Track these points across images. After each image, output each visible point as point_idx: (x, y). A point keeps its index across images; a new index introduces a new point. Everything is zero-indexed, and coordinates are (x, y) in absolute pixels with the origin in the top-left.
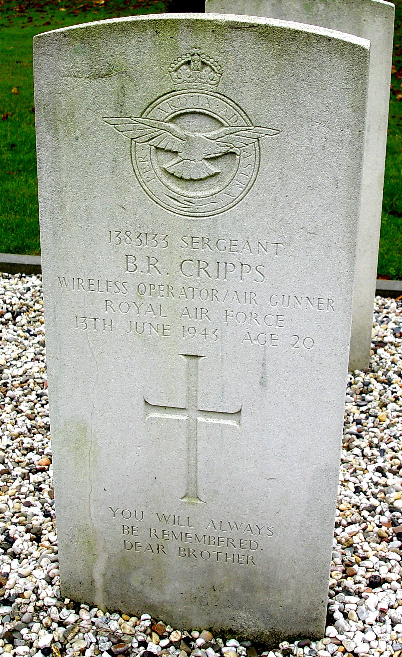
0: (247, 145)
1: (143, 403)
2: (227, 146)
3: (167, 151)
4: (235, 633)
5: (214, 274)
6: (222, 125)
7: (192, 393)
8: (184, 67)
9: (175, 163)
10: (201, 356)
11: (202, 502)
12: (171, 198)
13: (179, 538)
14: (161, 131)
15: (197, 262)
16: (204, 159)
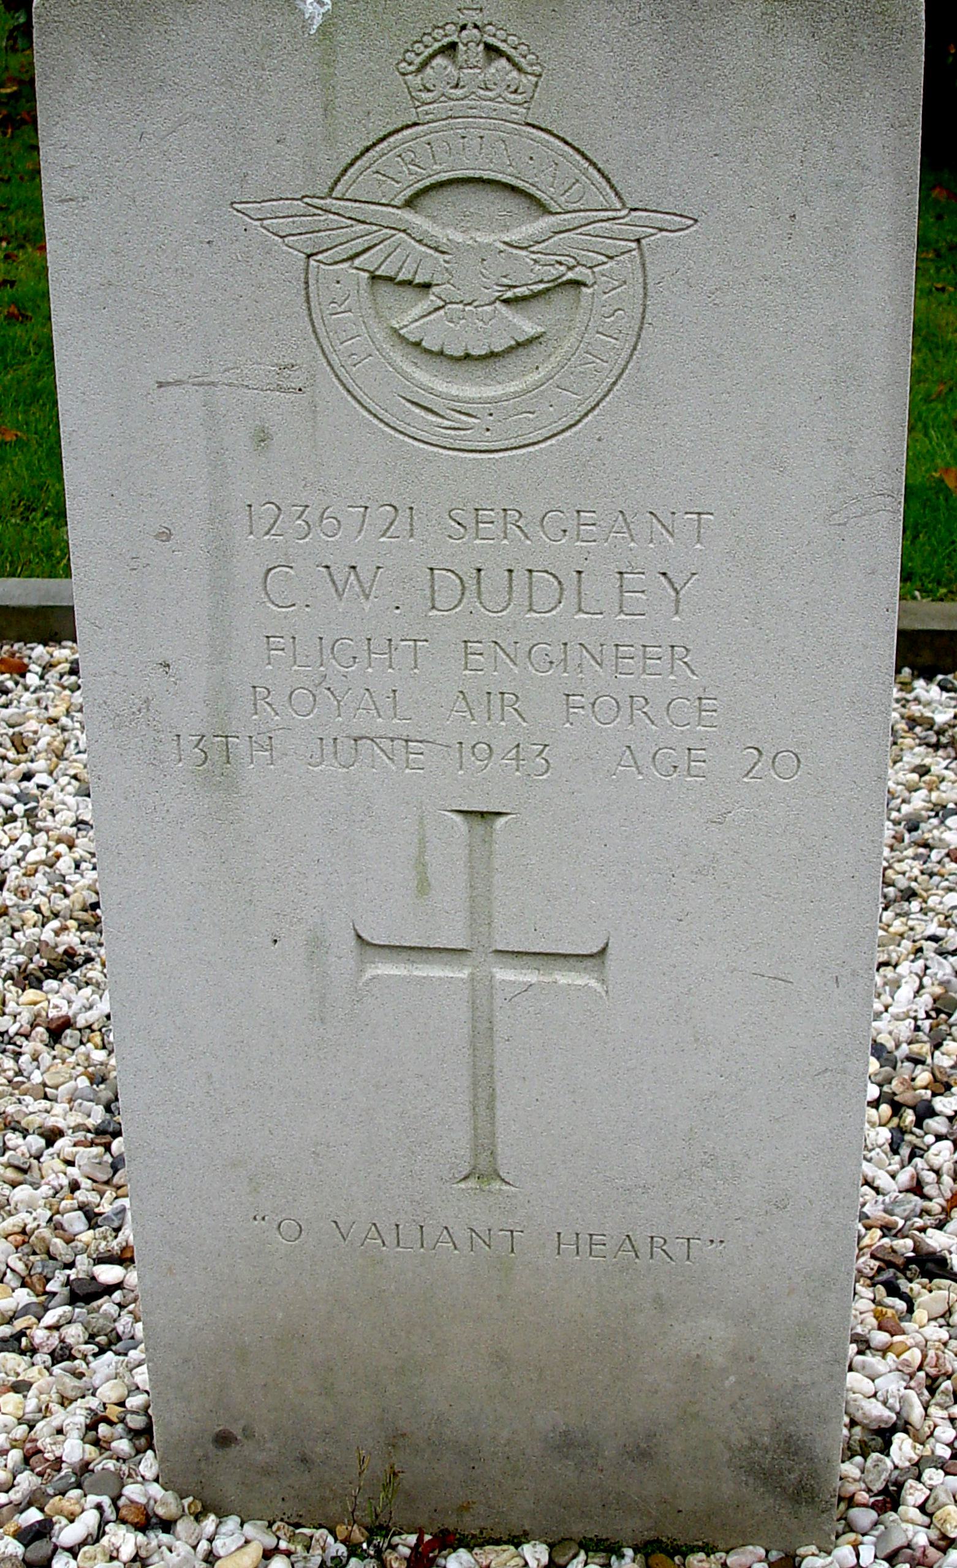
0: (611, 258)
1: (353, 942)
2: (560, 263)
7: (479, 911)
10: (499, 814)
12: (413, 403)
14: (387, 231)
15: (506, 573)
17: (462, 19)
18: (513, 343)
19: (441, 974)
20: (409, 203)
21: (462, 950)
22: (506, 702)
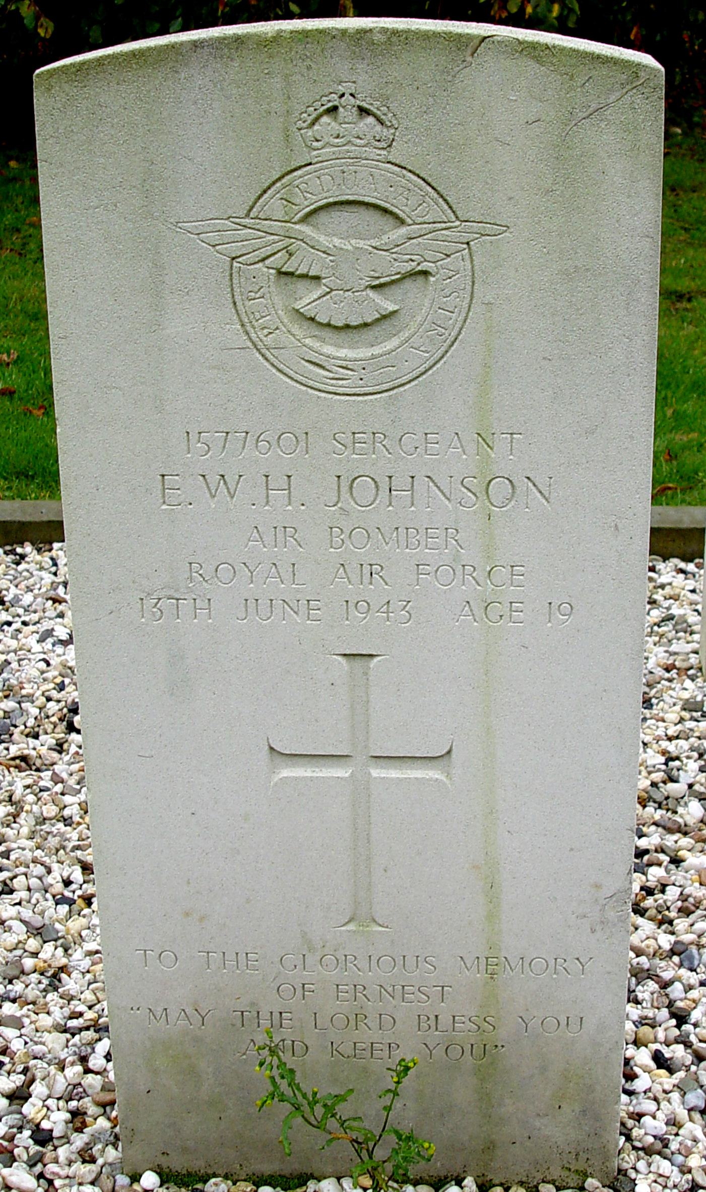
0: (448, 256)
1: (267, 748)
4: (446, 1177)
6: (402, 222)
8: (325, 119)
9: (315, 297)
11: (381, 929)
13: (475, 968)
14: (273, 237)
17: (341, 89)
18: (378, 316)
19: (309, 774)
20: (305, 219)
21: (347, 756)
22: (466, 572)
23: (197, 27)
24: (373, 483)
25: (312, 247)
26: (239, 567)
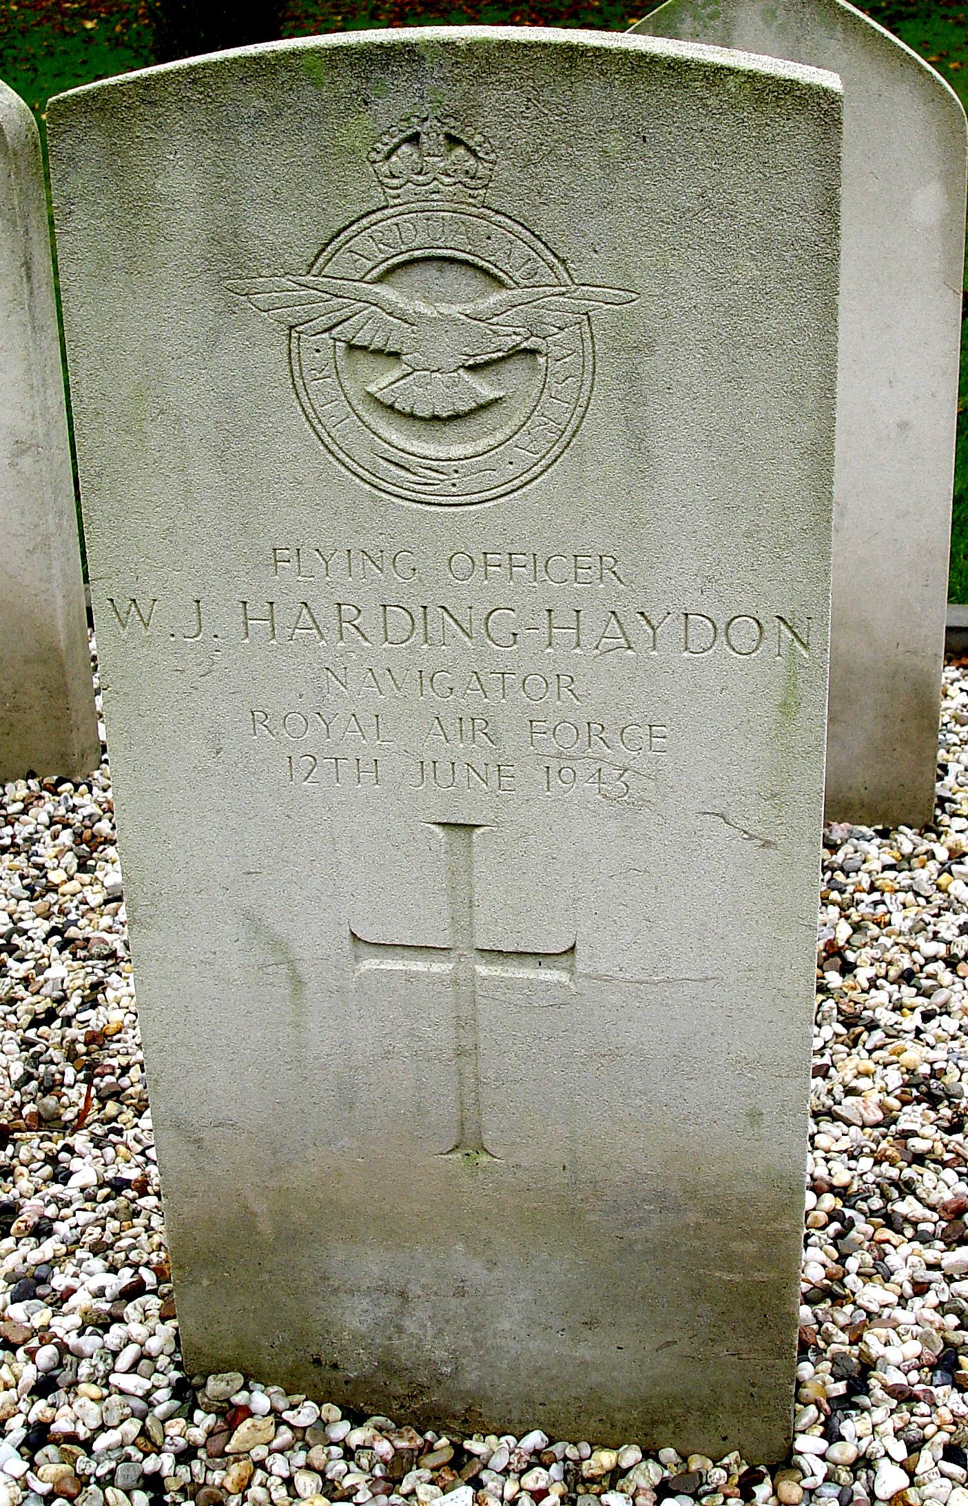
1: (348, 944)
2: (515, 333)
3: (372, 352)
5: (375, 633)
6: (502, 284)
15: (241, 605)
16: (463, 366)
23: (534, 23)
24: (755, 625)
25: (390, 314)
26: (312, 716)
